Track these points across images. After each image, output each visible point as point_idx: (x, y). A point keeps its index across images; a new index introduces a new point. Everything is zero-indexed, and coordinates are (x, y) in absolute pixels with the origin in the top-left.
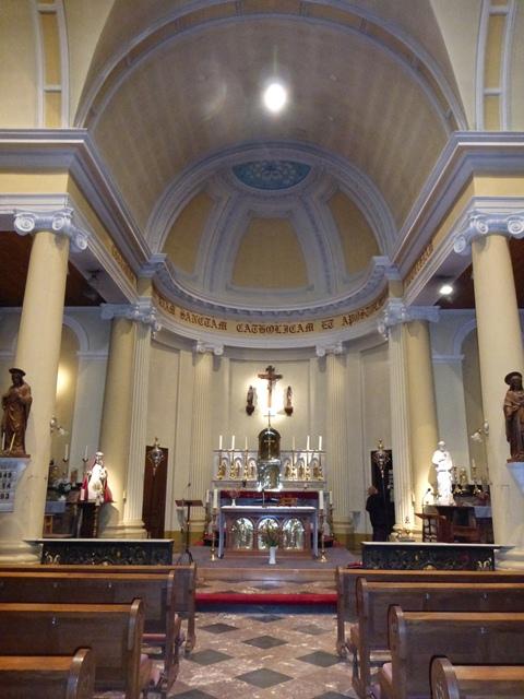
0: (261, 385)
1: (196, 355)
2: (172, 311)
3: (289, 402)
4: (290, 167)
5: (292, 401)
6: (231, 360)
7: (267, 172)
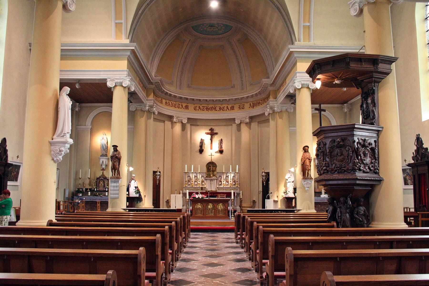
0: (207, 138)
1: (173, 123)
3: (221, 147)
4: (222, 25)
6: (191, 125)
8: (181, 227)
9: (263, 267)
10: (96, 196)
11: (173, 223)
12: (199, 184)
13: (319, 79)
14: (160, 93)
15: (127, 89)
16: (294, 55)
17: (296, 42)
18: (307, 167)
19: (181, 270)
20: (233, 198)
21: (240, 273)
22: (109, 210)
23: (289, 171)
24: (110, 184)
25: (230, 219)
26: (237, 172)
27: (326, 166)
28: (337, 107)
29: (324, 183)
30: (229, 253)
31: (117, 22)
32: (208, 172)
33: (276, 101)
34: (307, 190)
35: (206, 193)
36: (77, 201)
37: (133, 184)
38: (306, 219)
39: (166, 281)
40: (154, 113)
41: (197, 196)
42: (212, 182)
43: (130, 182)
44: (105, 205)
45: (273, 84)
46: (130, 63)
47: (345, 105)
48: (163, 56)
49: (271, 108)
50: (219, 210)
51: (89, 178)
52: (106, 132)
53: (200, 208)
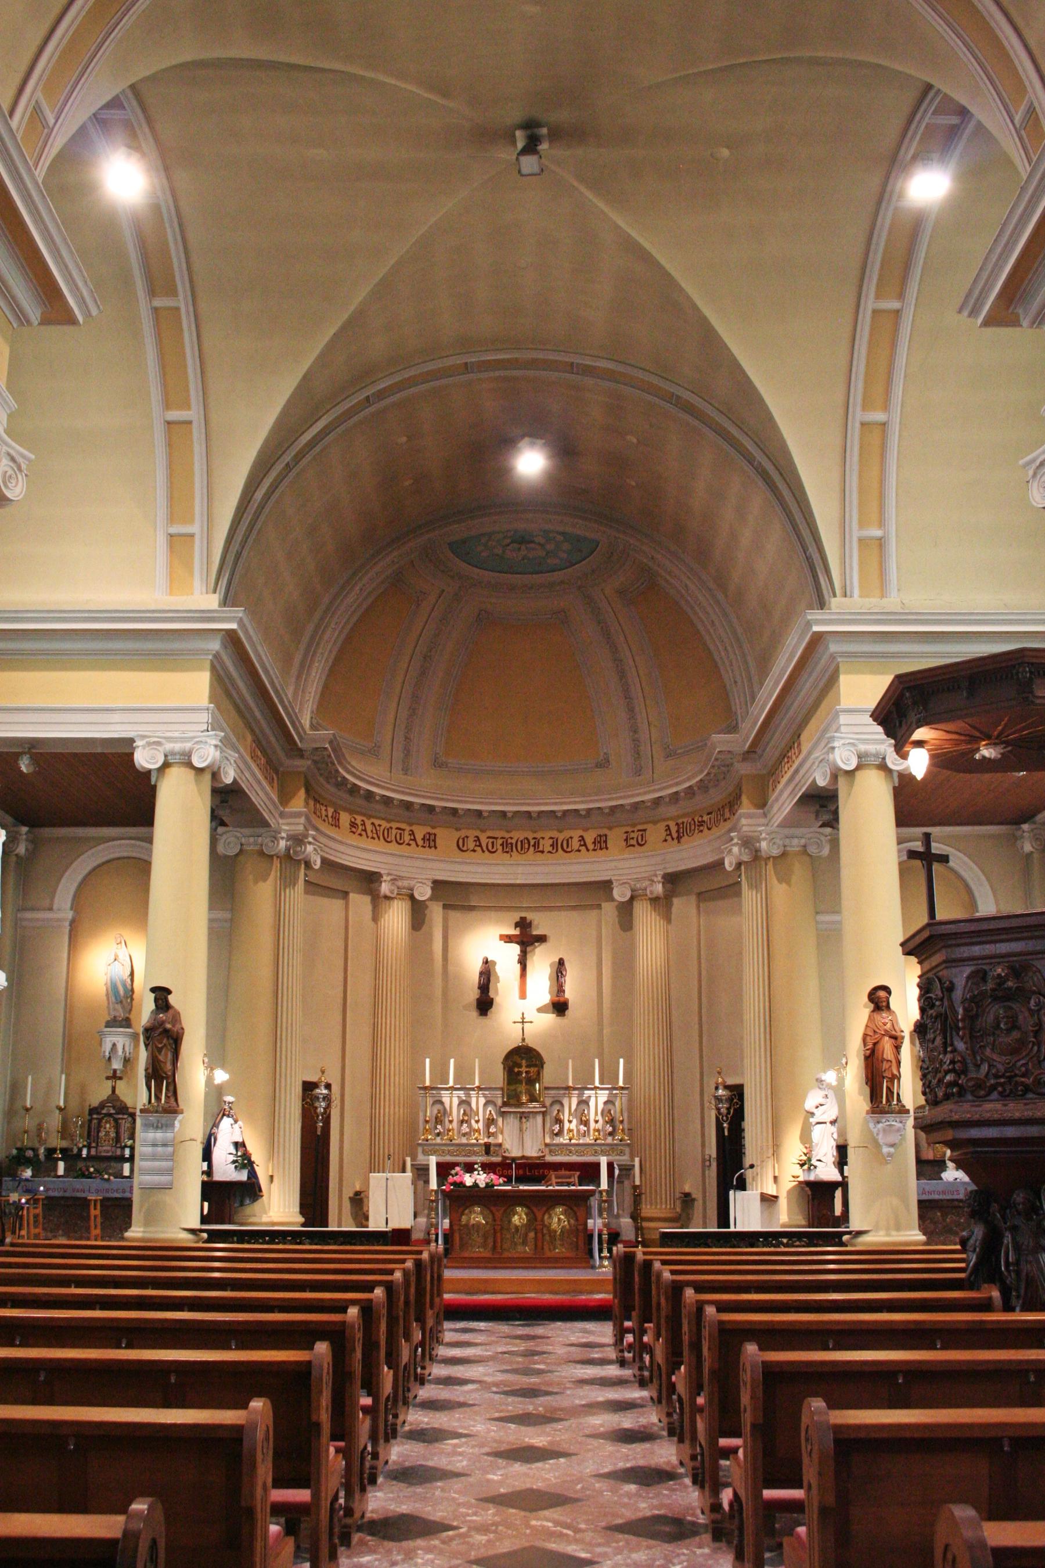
0: (506, 957)
1: (378, 901)
2: (336, 823)
3: (560, 989)
4: (560, 538)
5: (567, 988)
7: (516, 546)
8: (407, 1303)
9: (724, 1463)
10: (83, 1176)
11: (379, 1292)
12: (478, 1131)
13: (920, 744)
14: (333, 789)
15: (207, 777)
16: (827, 648)
17: (833, 600)
18: (885, 1065)
19: (408, 1475)
20: (604, 1185)
21: (633, 1487)
22: (136, 1232)
23: (820, 1081)
24: (139, 1133)
25: (593, 1267)
26: (621, 1084)
27: (953, 1070)
28: (991, 837)
29: (950, 1134)
30: (593, 1407)
31: (173, 530)
32: (509, 1083)
33: (765, 815)
34: (890, 1155)
35: (502, 1167)
36: (14, 1197)
37: (228, 1133)
38: (884, 1268)
39: (348, 1521)
40: (308, 865)
41: (468, 1180)
42: (527, 1125)
43: (216, 1125)
44: (119, 1211)
45: (750, 754)
46: (221, 682)
47: (1025, 827)
48: (341, 651)
49: (748, 842)
50: (552, 1233)
51: (60, 1109)
52: (127, 934)
53: (479, 1223)
